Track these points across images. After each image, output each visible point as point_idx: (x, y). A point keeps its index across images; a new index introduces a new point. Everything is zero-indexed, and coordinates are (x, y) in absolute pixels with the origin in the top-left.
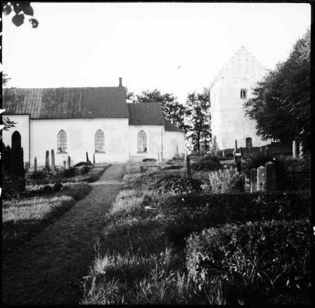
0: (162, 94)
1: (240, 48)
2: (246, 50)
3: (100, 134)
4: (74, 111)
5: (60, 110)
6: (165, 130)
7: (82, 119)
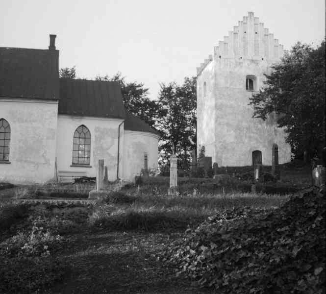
0: (127, 82)
1: (247, 15)
2: (256, 18)
6: (125, 128)
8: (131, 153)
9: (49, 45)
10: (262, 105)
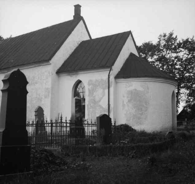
8: (125, 103)
9: (74, 15)
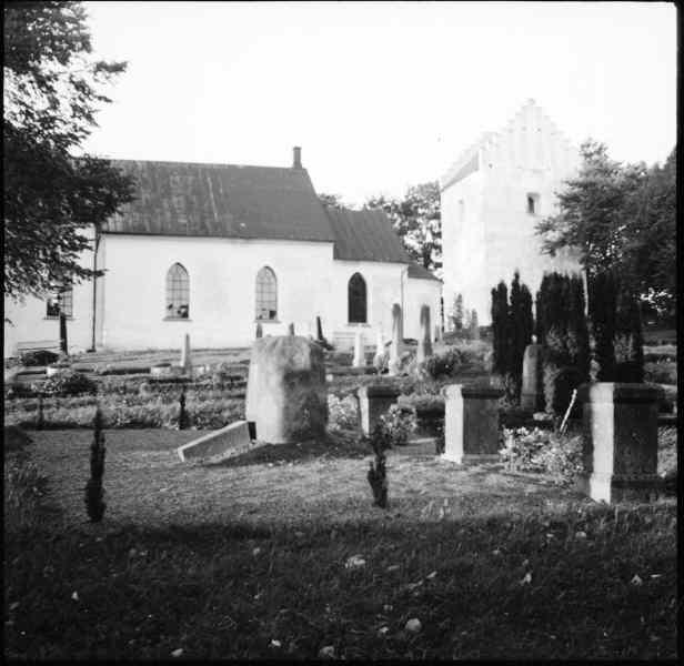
3: (267, 276)
4: (203, 218)
5: (168, 214)
7: (225, 240)
10: (553, 236)
